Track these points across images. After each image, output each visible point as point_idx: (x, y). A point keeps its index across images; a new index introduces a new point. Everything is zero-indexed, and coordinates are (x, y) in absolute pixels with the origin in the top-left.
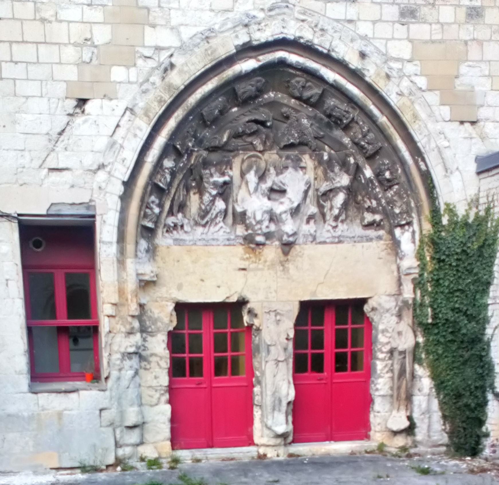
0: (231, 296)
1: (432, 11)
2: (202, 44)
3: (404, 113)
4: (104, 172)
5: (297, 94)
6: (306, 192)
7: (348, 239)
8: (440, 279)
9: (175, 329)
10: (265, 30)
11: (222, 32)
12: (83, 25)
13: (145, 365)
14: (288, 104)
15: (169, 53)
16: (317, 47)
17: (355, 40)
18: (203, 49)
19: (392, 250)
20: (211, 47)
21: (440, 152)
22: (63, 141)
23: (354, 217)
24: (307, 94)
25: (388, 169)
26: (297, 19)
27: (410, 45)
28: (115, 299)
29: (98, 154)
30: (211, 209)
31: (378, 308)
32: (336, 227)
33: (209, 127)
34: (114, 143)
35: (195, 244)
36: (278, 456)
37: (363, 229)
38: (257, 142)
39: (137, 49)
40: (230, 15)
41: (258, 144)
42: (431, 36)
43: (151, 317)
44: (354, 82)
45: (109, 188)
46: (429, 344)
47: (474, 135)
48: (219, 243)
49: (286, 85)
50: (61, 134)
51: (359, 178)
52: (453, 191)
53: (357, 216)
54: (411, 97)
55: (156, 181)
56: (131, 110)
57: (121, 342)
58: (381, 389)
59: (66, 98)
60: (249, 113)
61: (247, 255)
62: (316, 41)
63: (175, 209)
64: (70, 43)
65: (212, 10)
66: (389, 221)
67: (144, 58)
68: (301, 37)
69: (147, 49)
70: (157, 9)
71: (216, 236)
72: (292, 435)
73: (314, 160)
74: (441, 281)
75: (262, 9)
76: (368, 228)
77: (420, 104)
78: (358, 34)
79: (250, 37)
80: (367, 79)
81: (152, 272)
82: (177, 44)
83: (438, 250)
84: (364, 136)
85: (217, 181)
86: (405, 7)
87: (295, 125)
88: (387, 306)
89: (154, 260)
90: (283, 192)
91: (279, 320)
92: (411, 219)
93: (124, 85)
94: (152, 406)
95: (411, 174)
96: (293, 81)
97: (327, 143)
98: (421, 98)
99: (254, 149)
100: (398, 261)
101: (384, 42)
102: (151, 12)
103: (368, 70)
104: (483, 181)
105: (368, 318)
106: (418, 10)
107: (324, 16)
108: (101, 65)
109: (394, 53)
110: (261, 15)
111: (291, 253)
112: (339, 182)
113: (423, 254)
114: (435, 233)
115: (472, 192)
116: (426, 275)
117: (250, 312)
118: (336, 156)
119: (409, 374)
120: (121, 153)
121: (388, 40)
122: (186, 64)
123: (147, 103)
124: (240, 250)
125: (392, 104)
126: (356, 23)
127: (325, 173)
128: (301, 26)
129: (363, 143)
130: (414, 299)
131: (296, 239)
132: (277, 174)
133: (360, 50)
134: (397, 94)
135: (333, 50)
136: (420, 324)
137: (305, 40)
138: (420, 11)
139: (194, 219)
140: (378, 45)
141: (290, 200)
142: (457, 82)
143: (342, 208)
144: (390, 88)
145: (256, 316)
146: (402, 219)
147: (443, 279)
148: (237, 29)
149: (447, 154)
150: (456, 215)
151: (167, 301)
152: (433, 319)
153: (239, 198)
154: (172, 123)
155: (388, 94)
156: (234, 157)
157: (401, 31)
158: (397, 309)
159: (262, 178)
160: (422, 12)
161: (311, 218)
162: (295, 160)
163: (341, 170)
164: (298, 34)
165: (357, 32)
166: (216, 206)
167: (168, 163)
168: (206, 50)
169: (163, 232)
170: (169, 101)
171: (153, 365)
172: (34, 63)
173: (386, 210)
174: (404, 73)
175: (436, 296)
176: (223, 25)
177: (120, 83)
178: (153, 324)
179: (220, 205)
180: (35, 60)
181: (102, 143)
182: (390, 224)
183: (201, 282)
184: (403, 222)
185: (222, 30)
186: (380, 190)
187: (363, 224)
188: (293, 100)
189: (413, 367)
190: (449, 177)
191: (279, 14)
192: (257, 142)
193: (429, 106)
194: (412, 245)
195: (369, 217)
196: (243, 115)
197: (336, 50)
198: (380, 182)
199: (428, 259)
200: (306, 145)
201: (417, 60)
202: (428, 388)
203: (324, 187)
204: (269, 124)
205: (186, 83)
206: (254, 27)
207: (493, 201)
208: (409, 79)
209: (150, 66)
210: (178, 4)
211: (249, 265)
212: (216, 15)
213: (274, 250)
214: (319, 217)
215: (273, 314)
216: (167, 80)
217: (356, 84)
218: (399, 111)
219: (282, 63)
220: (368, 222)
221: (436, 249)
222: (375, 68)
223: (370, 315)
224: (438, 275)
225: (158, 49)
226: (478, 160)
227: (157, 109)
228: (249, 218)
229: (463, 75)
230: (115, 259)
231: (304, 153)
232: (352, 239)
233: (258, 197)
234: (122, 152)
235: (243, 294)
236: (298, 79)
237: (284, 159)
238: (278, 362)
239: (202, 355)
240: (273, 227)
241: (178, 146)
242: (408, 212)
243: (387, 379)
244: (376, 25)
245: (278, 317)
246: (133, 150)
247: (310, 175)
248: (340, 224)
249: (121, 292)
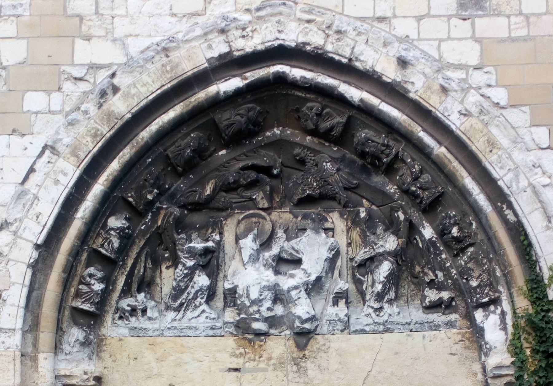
2: (157, 58)
3: (472, 139)
4: (8, 233)
11: (187, 41)
14: (301, 143)
15: (111, 72)
16: (330, 55)
17: (390, 43)
18: (159, 65)
19: (471, 342)
20: (170, 61)
21: (536, 193)
23: (411, 296)
24: (325, 125)
25: (455, 224)
26: (299, 19)
27: (477, 47)
30: (187, 287)
32: (381, 308)
33: (179, 175)
35: (162, 334)
37: (423, 312)
39: (63, 68)
40: (201, 20)
41: (259, 199)
42: (510, 33)
44: (393, 104)
48: (198, 332)
49: (296, 116)
51: (415, 241)
54: (482, 117)
55: (95, 246)
62: (329, 48)
63: (135, 286)
65: (174, 15)
67: (73, 81)
68: (305, 44)
69: (77, 68)
70: (94, 17)
71: (194, 323)
73: (347, 220)
75: (248, 10)
78: (394, 36)
79: (230, 46)
80: (412, 95)
81: (85, 373)
82: (124, 60)
83: (544, 339)
84: (416, 179)
87: (313, 170)
89: (99, 357)
90: (297, 262)
92: (497, 295)
93: (44, 115)
95: (490, 227)
97: (364, 194)
98: (499, 117)
100: (483, 358)
102: (84, 21)
103: (413, 83)
107: (342, 14)
108: (9, 90)
109: (451, 57)
112: (382, 246)
113: (519, 345)
114: (537, 313)
118: (379, 212)
120: (34, 205)
121: (441, 40)
123: (76, 138)
124: (230, 342)
125: (454, 128)
126: (390, 21)
128: (307, 28)
131: (317, 327)
132: (288, 239)
133: (397, 55)
134: (460, 113)
135: (357, 59)
137: (313, 46)
140: (426, 48)
143: (388, 281)
144: (449, 106)
146: (482, 296)
148: (210, 37)
154: (115, 166)
155: (446, 114)
156: (226, 219)
162: (317, 220)
163: (385, 230)
164: (301, 39)
165: (393, 33)
166: (195, 283)
167: (115, 222)
169: (114, 319)
173: (460, 285)
174: (469, 84)
177: (36, 113)
182: (467, 304)
184: (486, 300)
191: (272, 15)
193: (513, 128)
194: (503, 333)
195: (432, 295)
196: (234, 159)
197: (362, 58)
198: (446, 245)
199: (528, 352)
200: (333, 198)
203: (362, 255)
206: (234, 32)
209: (82, 91)
210: (125, 9)
211: (244, 364)
212: (180, 21)
216: (105, 107)
217: (397, 106)
219: (281, 79)
220: (430, 302)
221: (541, 337)
222: (423, 79)
224: (547, 377)
225: (94, 67)
228: (241, 296)
231: (332, 210)
232: (407, 326)
233: (258, 270)
234: (37, 205)
236: (309, 104)
237: (299, 219)
241: (130, 199)
242: (492, 285)
244: (422, 22)
246: (52, 201)
247: (341, 240)
248: (386, 306)
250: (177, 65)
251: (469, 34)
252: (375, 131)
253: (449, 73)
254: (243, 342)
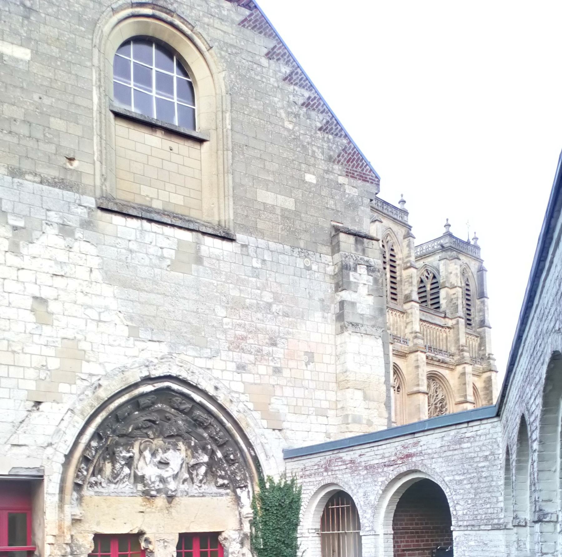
5: (177, 407)
6: (182, 465)
9: (93, 552)
11: (132, 369)
12: (41, 357)
15: (98, 378)
21: (263, 446)
22: (22, 427)
24: (183, 407)
25: (232, 454)
28: (55, 532)
29: (48, 437)
31: (229, 538)
32: (200, 487)
34: (60, 430)
39: (77, 374)
43: (77, 544)
45: (55, 459)
47: (281, 437)
50: (21, 423)
54: (245, 414)
56: (72, 410)
59: (27, 400)
61: (145, 503)
63: (96, 472)
64: (31, 367)
66: (233, 485)
68: (179, 376)
70: (91, 352)
71: (123, 490)
75: (157, 358)
80: (219, 402)
82: (104, 373)
84: (217, 434)
88: (234, 537)
90: (167, 464)
96: (174, 399)
99: (148, 437)
101: (228, 382)
104: (287, 464)
105: (221, 544)
110: (156, 361)
111: (173, 503)
115: (282, 469)
116: (258, 518)
117: (146, 540)
121: (230, 381)
122: (109, 385)
124: (140, 499)
125: (234, 417)
130: (251, 533)
136: (256, 549)
139: (108, 479)
142: (270, 407)
145: (150, 543)
146: (242, 483)
148: (141, 367)
149: (267, 447)
150: (274, 483)
153: (139, 466)
154: (98, 420)
156: (135, 441)
157: (238, 377)
158: (240, 539)
159: (154, 454)
161: (185, 480)
164: (178, 374)
170: (97, 407)
172: (6, 377)
176: (133, 364)
179: (126, 470)
180: (6, 376)
181: (51, 430)
188: (173, 410)
192: (150, 433)
195: (221, 481)
198: (227, 461)
199: (259, 508)
203: (192, 462)
204: (157, 422)
205: (109, 396)
207: (295, 476)
214: (189, 480)
215: (162, 542)
216: (96, 394)
218: (238, 421)
219: (168, 389)
222: (223, 395)
223: (223, 542)
225: (91, 375)
226: (285, 452)
227: (89, 411)
228: (147, 479)
229: (272, 403)
230: (57, 505)
236: (177, 398)
240: (161, 486)
242: (245, 479)
247: (183, 454)
248: (203, 485)
249: (60, 527)
250: (128, 379)
251: (240, 380)
252: (202, 412)
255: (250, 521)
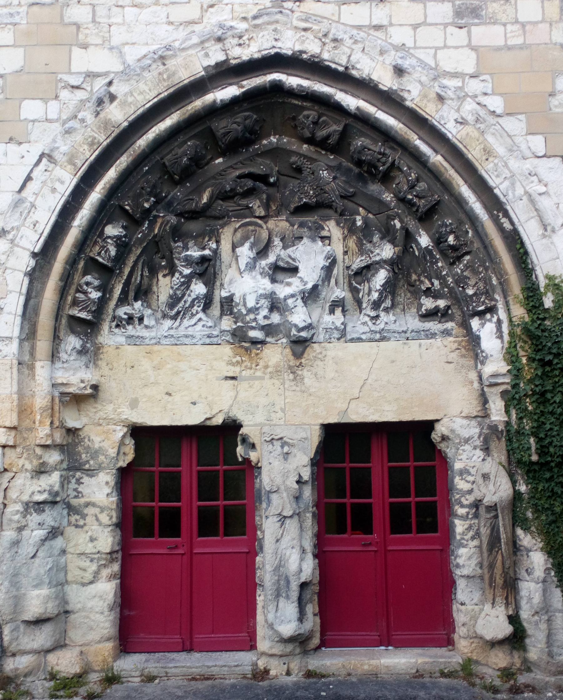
0: (214, 417)
1: (505, 7)
2: (154, 66)
3: (468, 147)
4: (5, 241)
7: (396, 335)
8: (546, 391)
10: (249, 46)
11: (184, 49)
13: (76, 520)
14: (297, 151)
15: (108, 80)
16: (327, 63)
17: (386, 52)
18: (155, 73)
19: (468, 350)
21: (532, 201)
23: (408, 305)
24: (321, 133)
25: (452, 232)
26: (296, 28)
27: (473, 55)
30: (183, 295)
31: (451, 436)
32: (377, 317)
35: (159, 342)
36: (288, 673)
37: (420, 320)
38: (256, 205)
40: (197, 28)
41: (255, 207)
42: (506, 41)
44: (390, 112)
46: (538, 496)
48: (194, 341)
49: (292, 124)
52: (558, 258)
53: (412, 303)
54: (478, 125)
55: (92, 255)
57: (24, 485)
58: (464, 566)
60: (241, 165)
61: (238, 358)
62: (326, 56)
63: (132, 294)
67: (71, 89)
68: (302, 52)
69: (74, 76)
70: (91, 25)
71: (190, 331)
72: (318, 635)
73: (343, 228)
74: (549, 396)
75: (245, 19)
76: (428, 319)
77: (493, 134)
78: (391, 44)
79: (227, 54)
80: (408, 103)
81: (82, 381)
82: (121, 68)
83: (540, 347)
84: (412, 187)
85: (191, 256)
86: (463, 4)
87: (309, 179)
88: (466, 434)
89: (96, 365)
90: (294, 270)
91: (287, 453)
92: (493, 303)
93: (40, 124)
94: (84, 585)
95: (486, 235)
97: (360, 202)
98: (495, 125)
100: (479, 366)
103: (409, 91)
105: (440, 451)
106: (484, 7)
107: (338, 22)
109: (447, 65)
111: (305, 355)
112: (378, 254)
113: (515, 353)
114: (533, 321)
117: (244, 440)
118: (376, 221)
119: (507, 544)
120: (31, 213)
121: (437, 49)
123: (73, 146)
124: (227, 351)
126: (386, 29)
127: (360, 245)
129: (410, 197)
130: (508, 424)
131: (313, 335)
132: (285, 247)
133: (394, 63)
135: (354, 68)
136: (519, 462)
138: (487, 8)
141: (302, 279)
144: (445, 115)
145: (253, 446)
147: (551, 391)
148: (206, 45)
149: (545, 203)
151: (115, 424)
152: (539, 455)
154: (111, 174)
155: (442, 122)
156: (222, 227)
160: (490, 10)
163: (382, 239)
164: (298, 48)
166: (191, 291)
167: (112, 230)
168: (160, 74)
169: (111, 327)
171: (89, 519)
173: (456, 293)
174: (465, 92)
175: (542, 419)
177: (34, 121)
178: (92, 458)
182: (463, 312)
183: (167, 396)
184: (482, 308)
185: (183, 46)
186: (444, 265)
187: (420, 313)
189: (514, 532)
190: (550, 237)
191: (269, 23)
193: (509, 136)
194: (499, 341)
195: (428, 303)
196: (231, 167)
197: (358, 66)
198: (443, 253)
199: (524, 360)
200: (329, 206)
201: (485, 74)
202: (542, 569)
203: (358, 263)
206: (231, 40)
208: (475, 101)
210: (122, 18)
211: (241, 372)
212: (177, 29)
213: (280, 349)
215: (278, 444)
216: (102, 115)
220: (426, 310)
221: (537, 346)
222: (419, 87)
225: (91, 75)
228: (238, 304)
232: (403, 334)
234: (34, 213)
235: (231, 414)
236: (306, 113)
237: (296, 227)
238: (283, 519)
239: (180, 504)
241: (127, 208)
242: (488, 293)
243: (473, 550)
244: (418, 30)
245: (286, 449)
246: (49, 210)
247: (338, 248)
248: (382, 314)
250: (174, 74)
251: (465, 43)
252: (372, 139)
253: (446, 82)
254: (239, 350)
255: (504, 394)
